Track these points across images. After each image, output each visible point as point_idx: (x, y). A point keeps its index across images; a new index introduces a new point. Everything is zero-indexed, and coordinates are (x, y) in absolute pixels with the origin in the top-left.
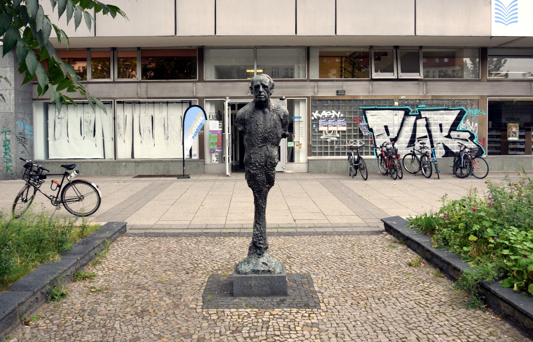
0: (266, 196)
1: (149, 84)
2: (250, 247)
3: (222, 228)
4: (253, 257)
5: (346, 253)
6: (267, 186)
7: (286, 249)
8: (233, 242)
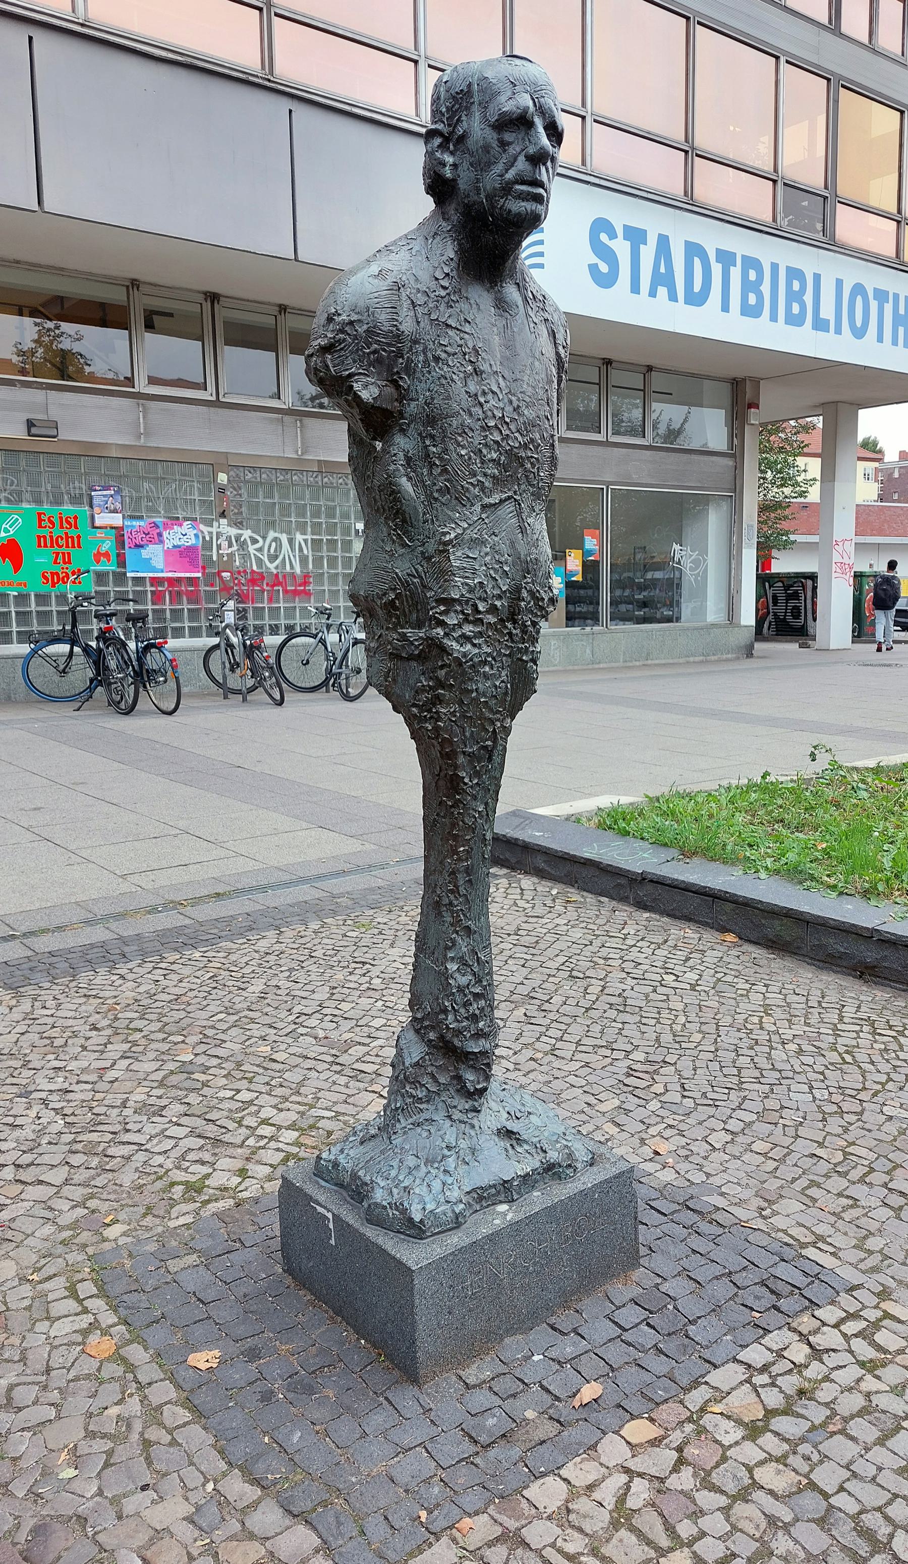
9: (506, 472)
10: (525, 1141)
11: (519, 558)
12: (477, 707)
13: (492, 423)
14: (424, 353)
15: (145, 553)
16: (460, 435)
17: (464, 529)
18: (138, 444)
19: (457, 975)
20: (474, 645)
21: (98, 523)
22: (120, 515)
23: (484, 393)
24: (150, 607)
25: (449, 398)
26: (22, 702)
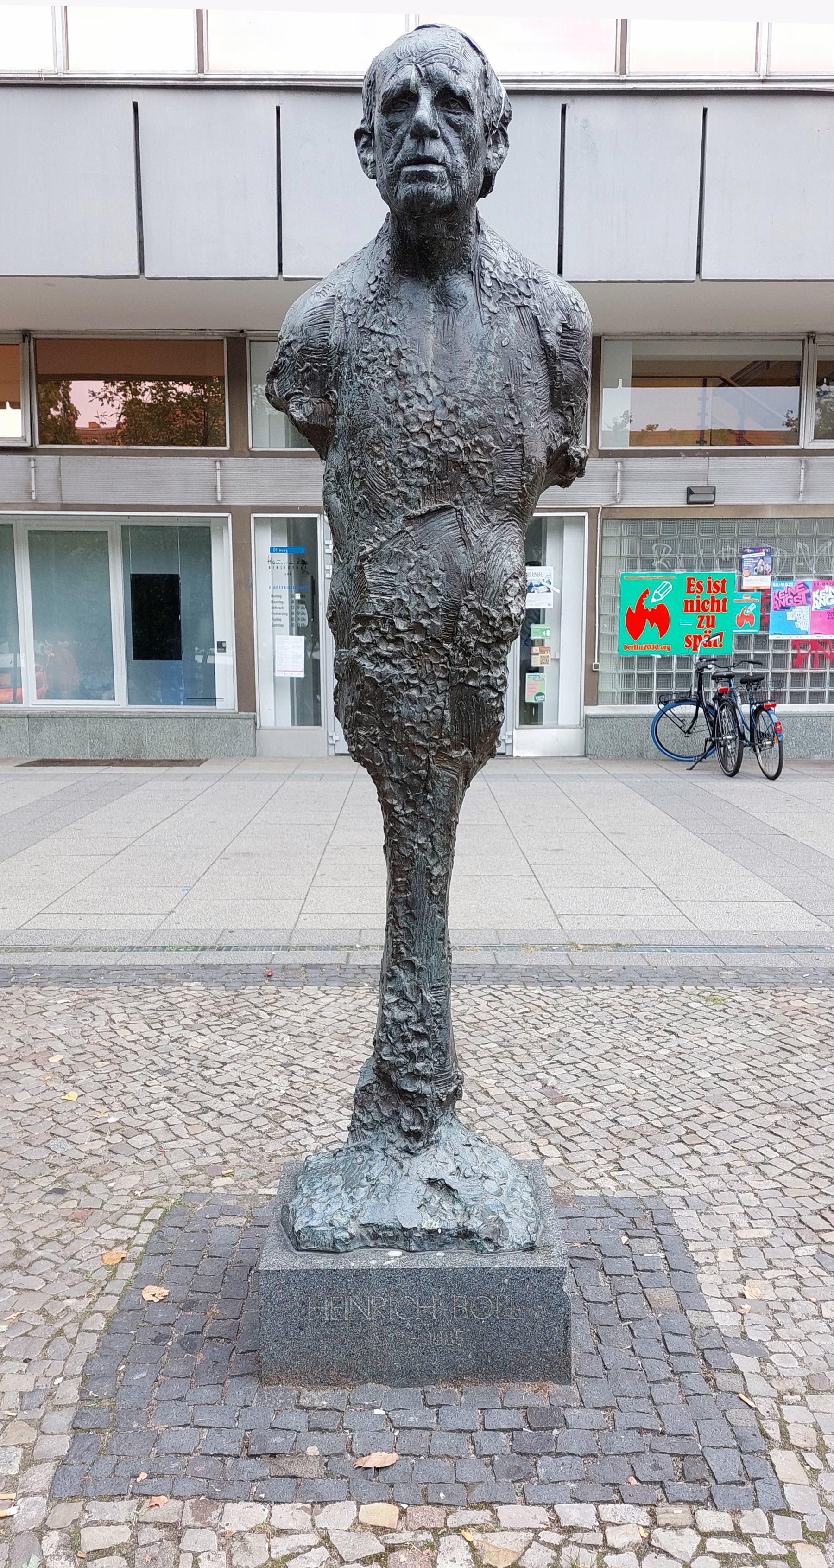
0: (454, 812)
1: (65, 459)
2: (364, 1089)
3: (278, 948)
4: (377, 1148)
5: (806, 1076)
6: (455, 754)
7: (536, 1051)
8: (313, 1008)
9: (441, 480)
10: (459, 1201)
11: (458, 573)
12: (402, 731)
13: (416, 429)
14: (349, 365)
15: (790, 615)
16: (377, 445)
17: (382, 544)
18: (796, 502)
19: (395, 1008)
20: (394, 666)
21: (746, 585)
22: (769, 577)
23: (407, 398)
24: (790, 670)
25: (366, 407)
26: (651, 759)
